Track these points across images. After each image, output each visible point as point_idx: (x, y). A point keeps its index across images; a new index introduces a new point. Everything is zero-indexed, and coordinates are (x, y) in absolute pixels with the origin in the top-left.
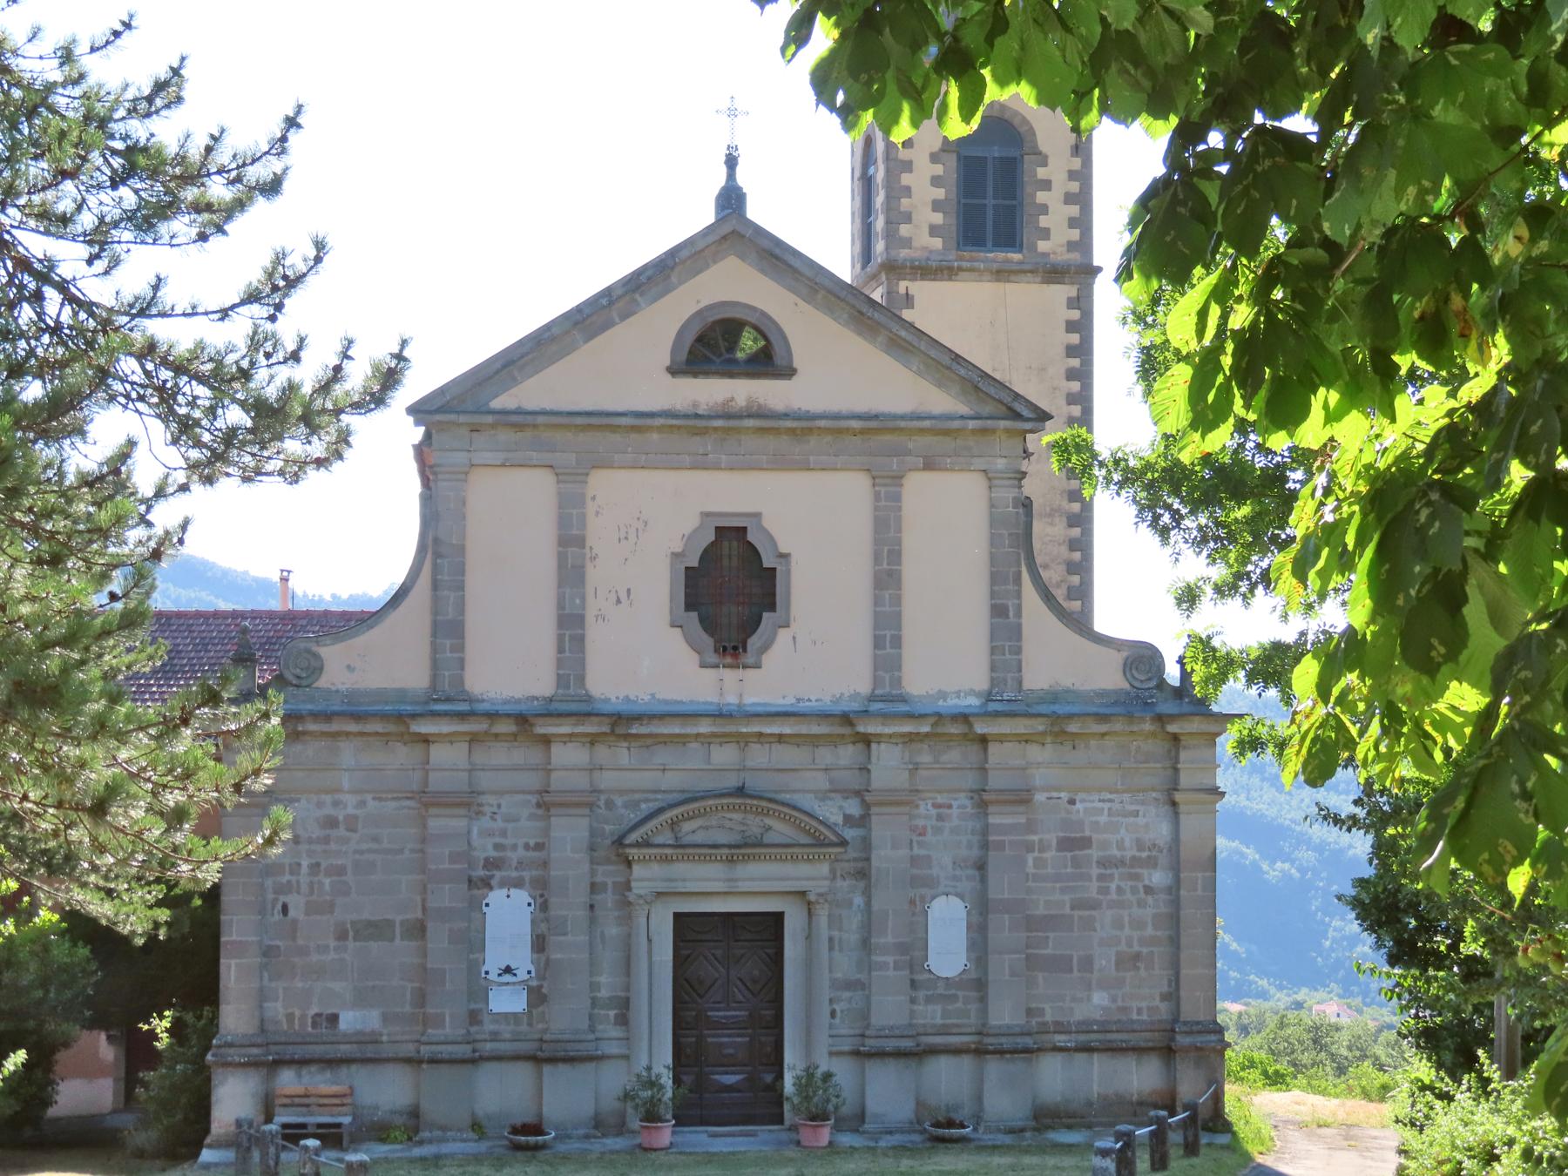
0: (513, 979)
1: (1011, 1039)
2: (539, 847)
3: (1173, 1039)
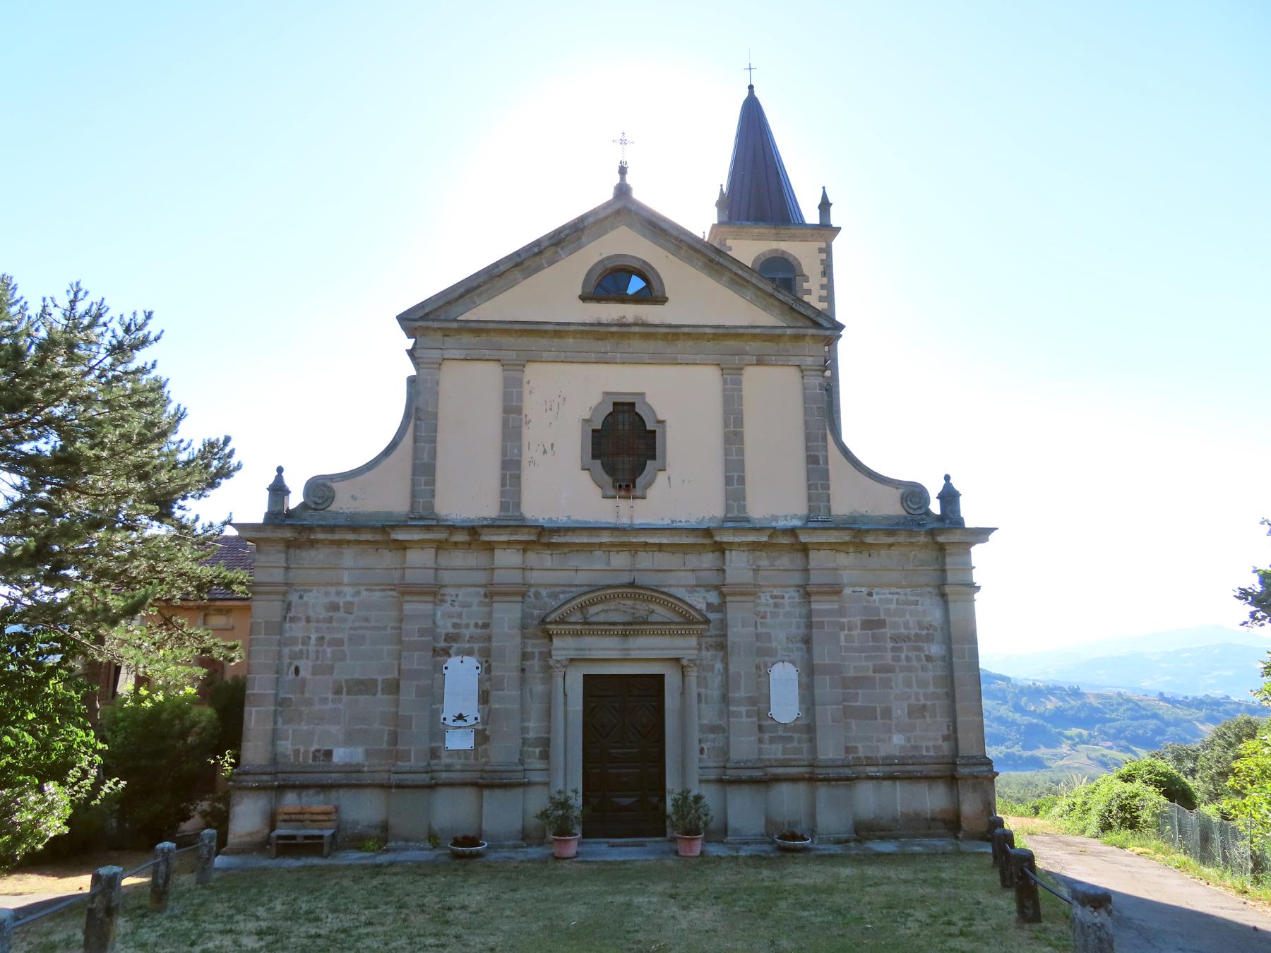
0: (464, 724)
1: (835, 770)
2: (486, 626)
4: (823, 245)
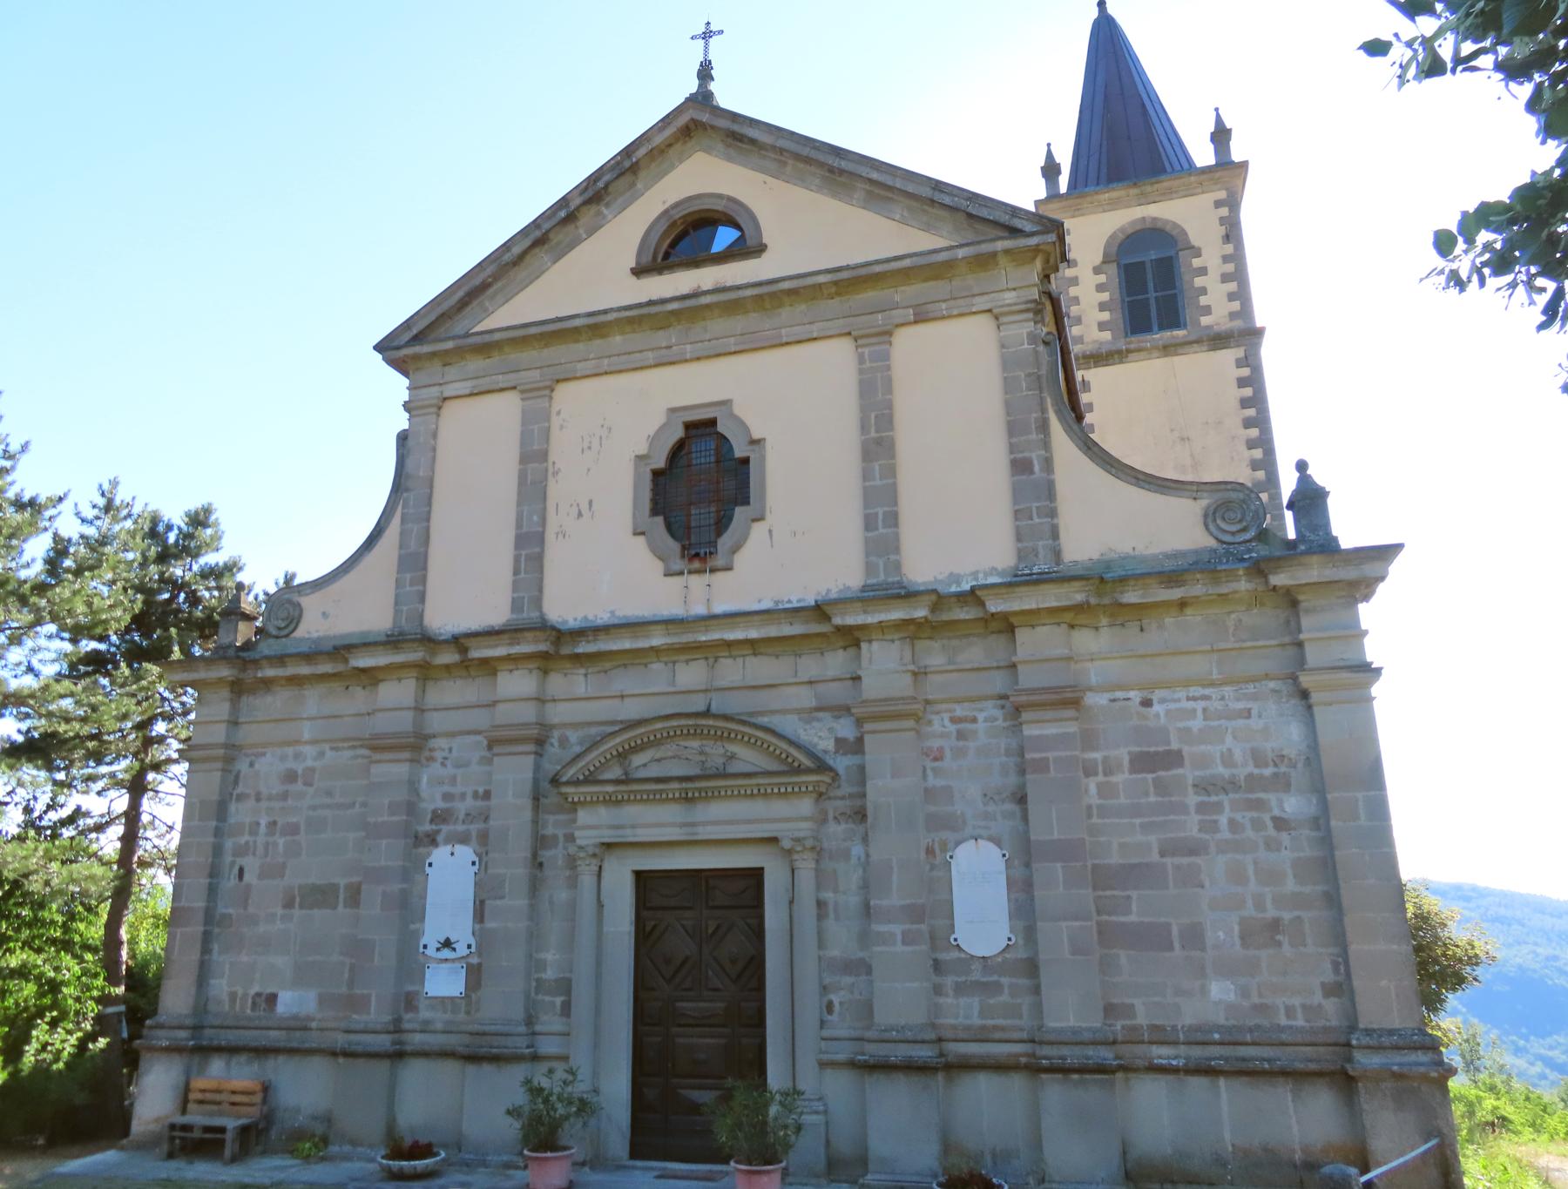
1: (1077, 1050)
2: (487, 795)
3: (1350, 1059)
4: (1222, 195)
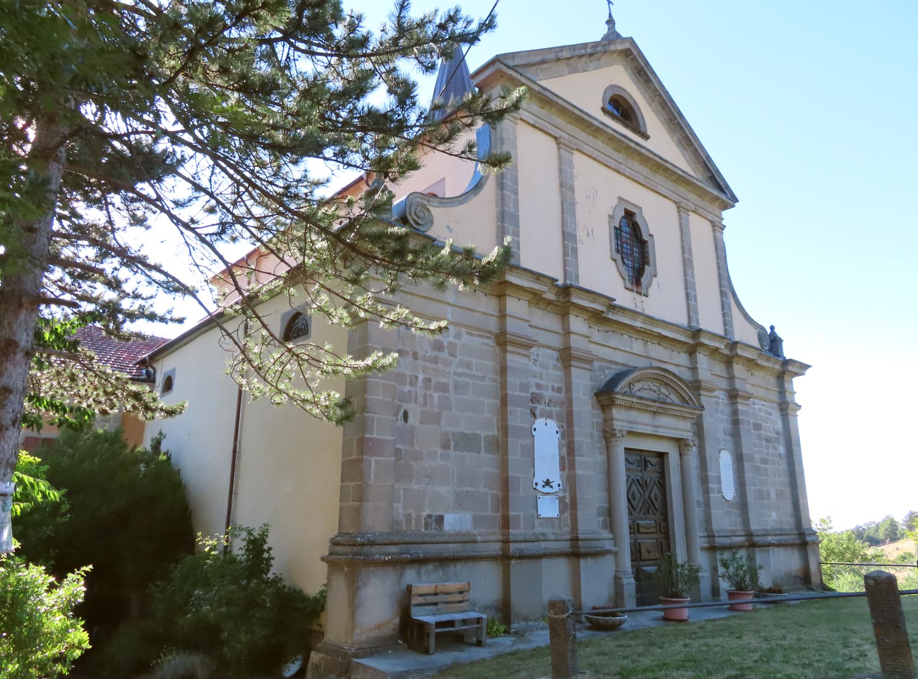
0: (551, 490)
